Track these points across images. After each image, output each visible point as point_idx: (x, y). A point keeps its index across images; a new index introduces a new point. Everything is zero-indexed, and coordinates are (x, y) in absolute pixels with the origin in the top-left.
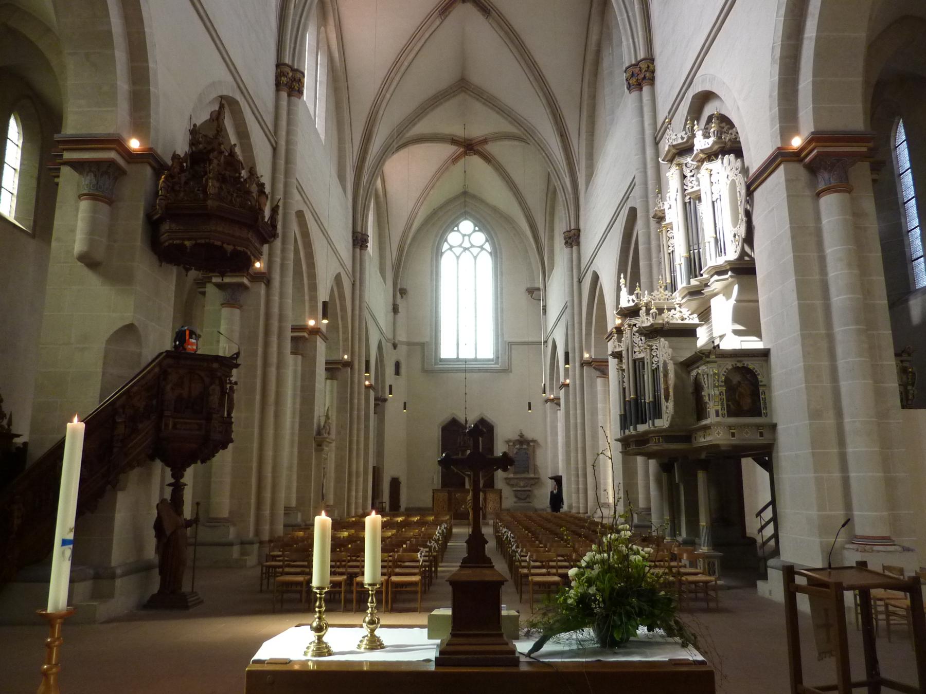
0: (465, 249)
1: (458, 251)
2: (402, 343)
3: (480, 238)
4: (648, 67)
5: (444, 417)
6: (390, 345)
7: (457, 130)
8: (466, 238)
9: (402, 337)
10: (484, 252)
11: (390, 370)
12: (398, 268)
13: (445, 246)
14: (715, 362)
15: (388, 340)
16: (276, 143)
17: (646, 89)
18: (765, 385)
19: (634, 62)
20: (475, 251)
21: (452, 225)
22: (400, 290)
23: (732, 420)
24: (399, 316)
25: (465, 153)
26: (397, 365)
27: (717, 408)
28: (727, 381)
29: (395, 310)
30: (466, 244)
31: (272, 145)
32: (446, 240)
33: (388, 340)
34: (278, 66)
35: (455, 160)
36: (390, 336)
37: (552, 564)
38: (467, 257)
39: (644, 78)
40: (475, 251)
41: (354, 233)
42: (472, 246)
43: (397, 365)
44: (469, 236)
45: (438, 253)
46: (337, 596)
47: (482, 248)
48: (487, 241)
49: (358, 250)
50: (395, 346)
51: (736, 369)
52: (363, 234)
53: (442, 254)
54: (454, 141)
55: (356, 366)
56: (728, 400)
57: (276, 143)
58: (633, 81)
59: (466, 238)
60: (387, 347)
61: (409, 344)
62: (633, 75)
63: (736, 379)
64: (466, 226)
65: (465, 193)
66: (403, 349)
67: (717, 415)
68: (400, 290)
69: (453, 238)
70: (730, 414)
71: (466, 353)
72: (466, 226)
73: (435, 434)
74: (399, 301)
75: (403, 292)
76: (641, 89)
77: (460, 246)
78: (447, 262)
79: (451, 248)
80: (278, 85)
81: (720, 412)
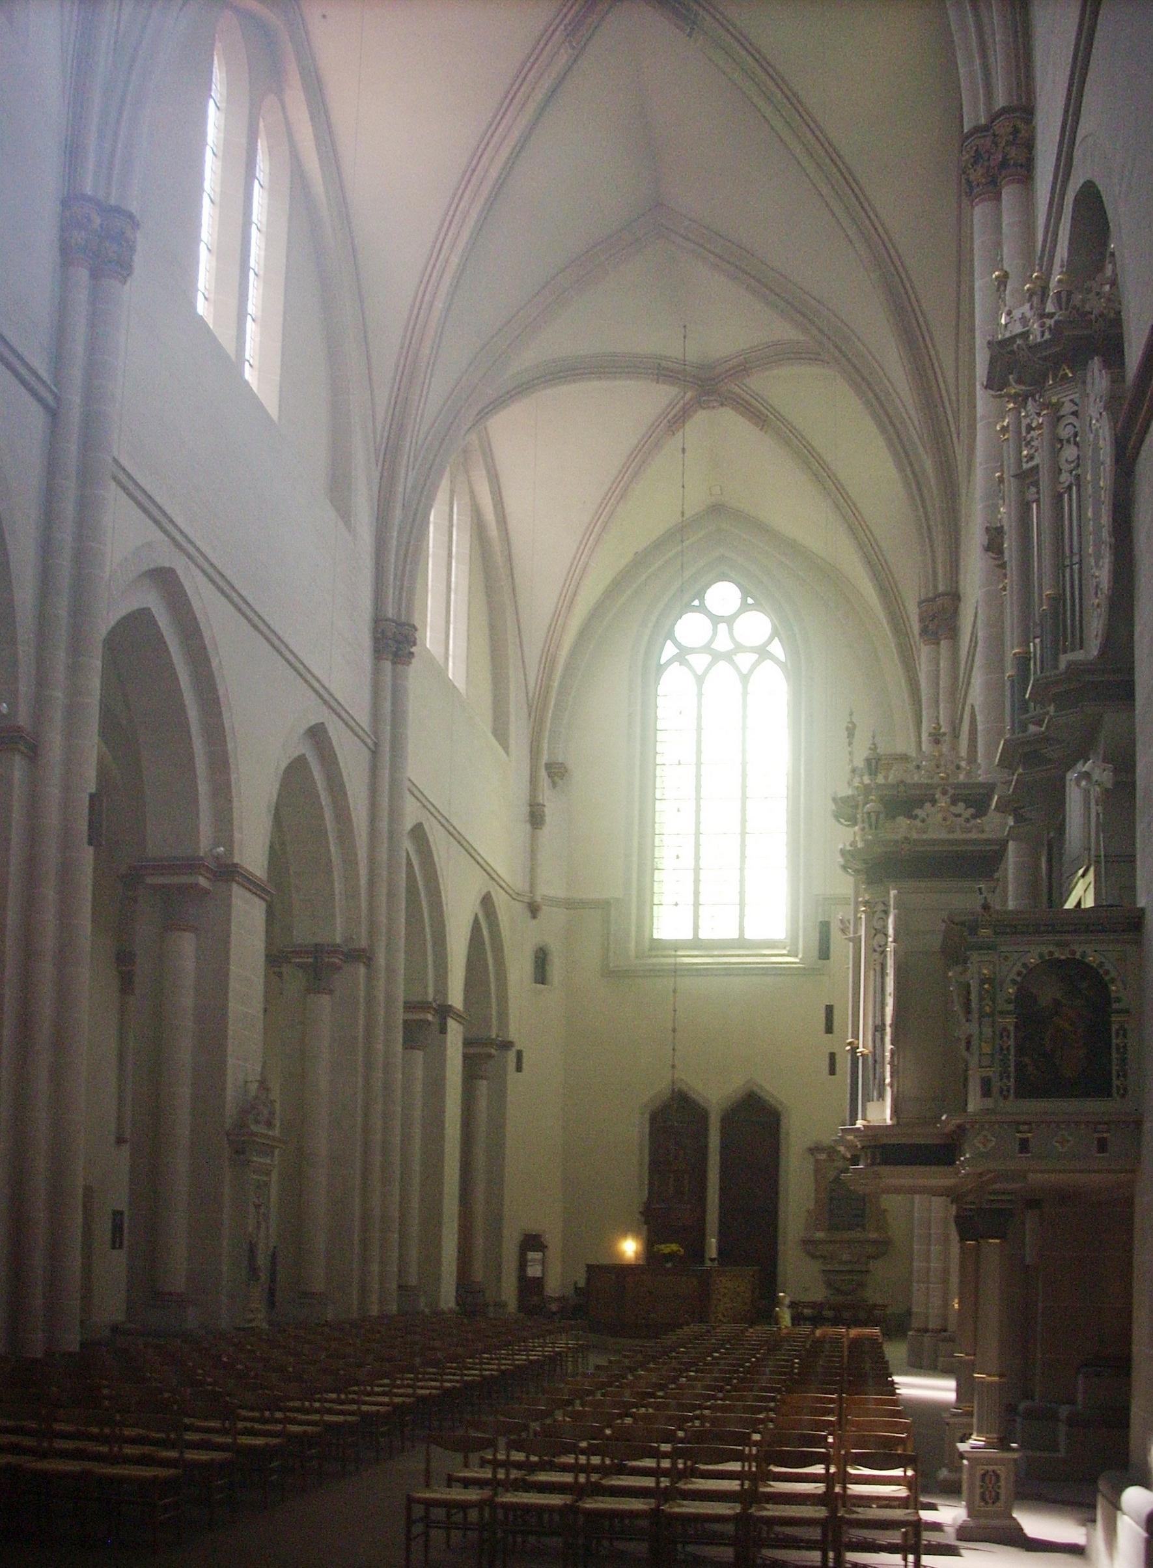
0: (717, 656)
1: (699, 661)
2: (554, 902)
3: (757, 626)
4: (1016, 131)
5: (656, 1087)
6: (519, 908)
7: (658, 340)
8: (722, 627)
9: (551, 886)
10: (768, 664)
11: (519, 969)
12: (537, 713)
13: (669, 650)
14: (991, 947)
15: (514, 896)
16: (57, 398)
17: (1009, 194)
18: (1127, 1011)
19: (983, 121)
20: (745, 660)
21: (689, 595)
22: (548, 766)
23: (1034, 1107)
24: (546, 831)
25: (698, 403)
26: (541, 960)
27: (989, 1072)
28: (1024, 999)
29: (536, 818)
30: (723, 643)
31: (46, 407)
32: (670, 635)
33: (514, 896)
34: (65, 203)
35: (677, 420)
36: (518, 882)
37: (189, 1436)
38: (723, 675)
39: (1004, 164)
40: (745, 660)
41: (378, 621)
42: (739, 648)
43: (541, 960)
44: (730, 620)
45: (651, 671)
46: (438, 1513)
47: (762, 652)
48: (775, 633)
49: (387, 665)
50: (534, 910)
51: (1052, 965)
52: (400, 624)
53: (660, 669)
54: (663, 371)
55: (381, 960)
56: (1020, 1050)
57: (57, 398)
58: (977, 175)
59: (722, 627)
60: (508, 912)
61: (570, 904)
62: (976, 159)
63: (1048, 993)
64: (723, 595)
65: (717, 509)
66: (553, 920)
67: (986, 1092)
68: (548, 766)
69: (690, 628)
70: (1027, 1089)
71: (718, 926)
72: (723, 595)
73: (629, 1133)
74: (546, 795)
75: (557, 772)
76: (998, 197)
77: (707, 648)
78: (673, 690)
79: (762, 652)
80: (66, 252)
81: (996, 1085)
